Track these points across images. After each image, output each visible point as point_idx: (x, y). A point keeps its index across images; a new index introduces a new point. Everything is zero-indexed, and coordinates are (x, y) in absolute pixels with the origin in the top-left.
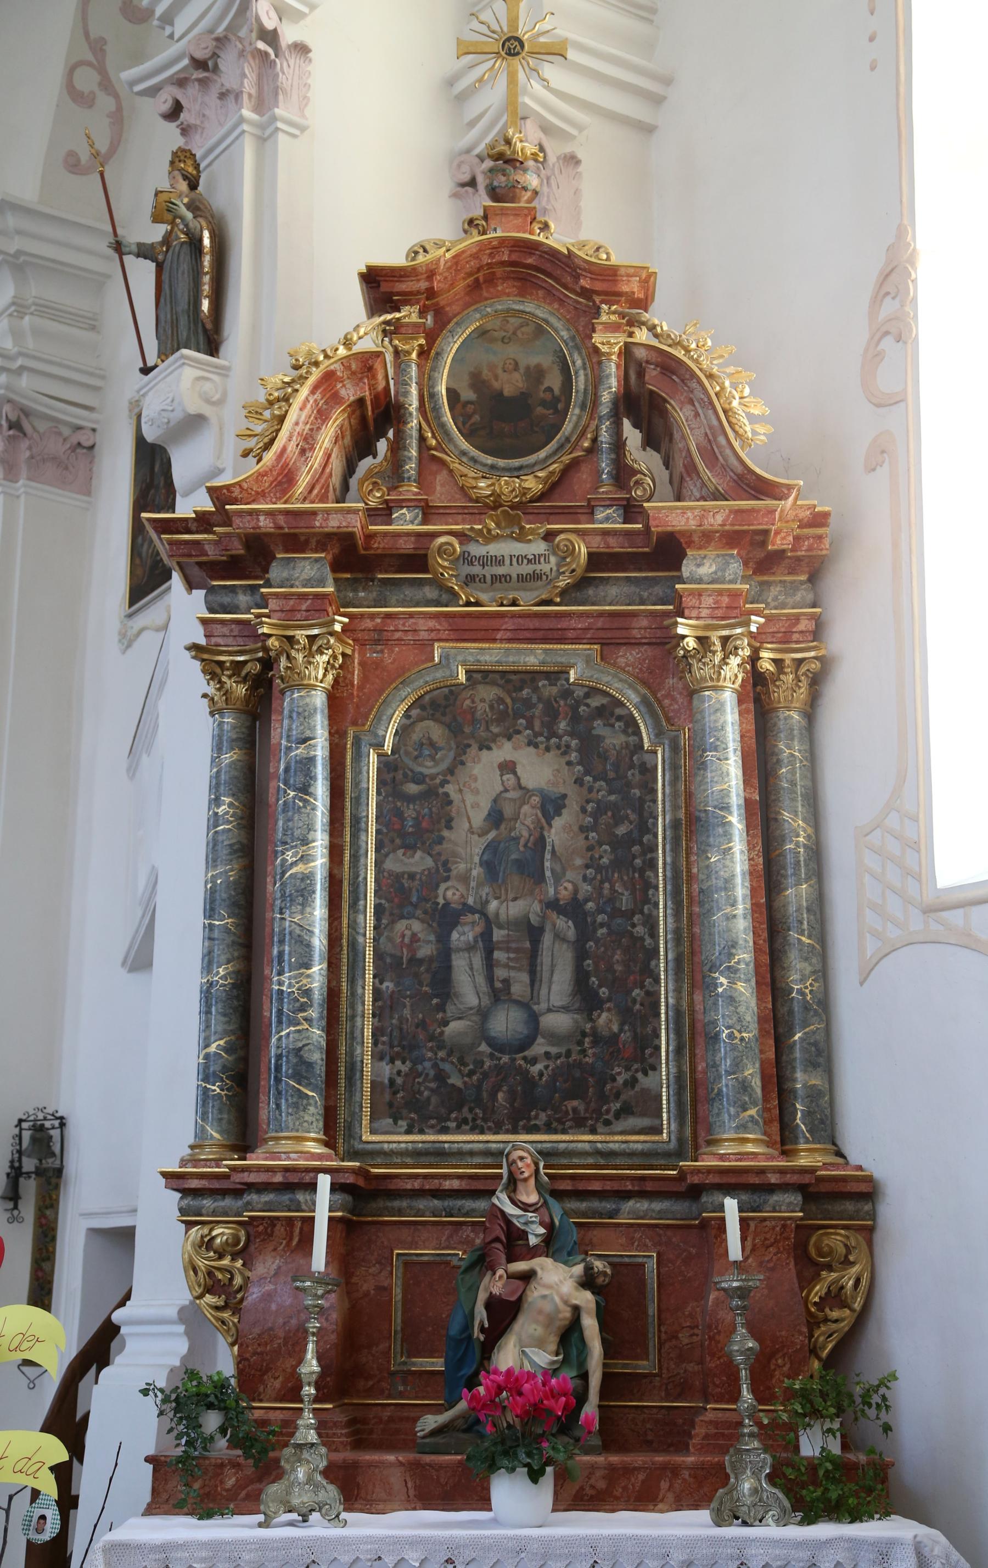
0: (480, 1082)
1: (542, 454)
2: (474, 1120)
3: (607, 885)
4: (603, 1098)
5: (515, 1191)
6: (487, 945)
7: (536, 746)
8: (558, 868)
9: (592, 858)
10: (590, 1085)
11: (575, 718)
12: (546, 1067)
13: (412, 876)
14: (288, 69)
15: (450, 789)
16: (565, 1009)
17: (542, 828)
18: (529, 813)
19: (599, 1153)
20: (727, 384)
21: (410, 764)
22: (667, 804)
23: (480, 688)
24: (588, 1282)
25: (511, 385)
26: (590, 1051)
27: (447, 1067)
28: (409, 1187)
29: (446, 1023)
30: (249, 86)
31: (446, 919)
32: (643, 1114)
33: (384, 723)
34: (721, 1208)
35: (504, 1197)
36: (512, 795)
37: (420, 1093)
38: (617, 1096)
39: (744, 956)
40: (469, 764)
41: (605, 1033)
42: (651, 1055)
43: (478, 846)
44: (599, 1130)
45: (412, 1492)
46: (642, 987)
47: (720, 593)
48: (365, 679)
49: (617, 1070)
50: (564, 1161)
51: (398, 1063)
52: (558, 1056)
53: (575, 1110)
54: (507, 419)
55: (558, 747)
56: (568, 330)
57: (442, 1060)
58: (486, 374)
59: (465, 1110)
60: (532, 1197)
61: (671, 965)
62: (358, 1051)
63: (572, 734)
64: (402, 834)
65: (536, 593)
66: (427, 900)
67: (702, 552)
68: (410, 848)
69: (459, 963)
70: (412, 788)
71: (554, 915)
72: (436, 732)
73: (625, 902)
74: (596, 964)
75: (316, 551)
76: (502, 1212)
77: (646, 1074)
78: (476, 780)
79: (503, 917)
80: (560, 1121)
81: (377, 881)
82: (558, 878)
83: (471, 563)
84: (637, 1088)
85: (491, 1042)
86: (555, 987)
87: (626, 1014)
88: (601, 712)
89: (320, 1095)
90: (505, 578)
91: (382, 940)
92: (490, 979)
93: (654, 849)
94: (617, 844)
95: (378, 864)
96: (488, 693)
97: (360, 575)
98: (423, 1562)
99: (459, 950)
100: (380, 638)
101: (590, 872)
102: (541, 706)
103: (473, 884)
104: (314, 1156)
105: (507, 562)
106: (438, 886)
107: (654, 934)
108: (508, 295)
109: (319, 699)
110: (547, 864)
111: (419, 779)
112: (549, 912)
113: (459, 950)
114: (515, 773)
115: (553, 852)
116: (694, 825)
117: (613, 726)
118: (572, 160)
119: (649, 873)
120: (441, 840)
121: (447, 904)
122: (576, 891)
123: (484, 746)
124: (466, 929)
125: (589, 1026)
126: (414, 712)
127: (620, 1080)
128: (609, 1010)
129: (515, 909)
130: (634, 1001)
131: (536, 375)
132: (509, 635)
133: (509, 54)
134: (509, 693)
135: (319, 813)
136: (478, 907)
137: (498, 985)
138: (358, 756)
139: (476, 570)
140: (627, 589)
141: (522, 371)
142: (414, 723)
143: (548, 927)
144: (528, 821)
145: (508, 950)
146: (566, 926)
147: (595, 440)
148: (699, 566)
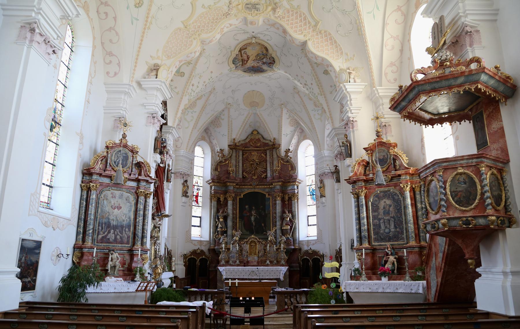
6: (384, 222)
10: (396, 237)
14: (355, 124)
18: (388, 207)
24: (395, 258)
25: (382, 157)
30: (351, 127)
31: (380, 219)
39: (412, 221)
43: (382, 211)
60: (389, 249)
69: (381, 224)
72: (377, 199)
73: (399, 216)
87: (400, 229)
88: (395, 195)
94: (398, 210)
96: (382, 194)
100: (370, 189)
109: (363, 197)
116: (405, 207)
118: (478, 31)
129: (387, 218)
131: (384, 156)
146: (393, 219)
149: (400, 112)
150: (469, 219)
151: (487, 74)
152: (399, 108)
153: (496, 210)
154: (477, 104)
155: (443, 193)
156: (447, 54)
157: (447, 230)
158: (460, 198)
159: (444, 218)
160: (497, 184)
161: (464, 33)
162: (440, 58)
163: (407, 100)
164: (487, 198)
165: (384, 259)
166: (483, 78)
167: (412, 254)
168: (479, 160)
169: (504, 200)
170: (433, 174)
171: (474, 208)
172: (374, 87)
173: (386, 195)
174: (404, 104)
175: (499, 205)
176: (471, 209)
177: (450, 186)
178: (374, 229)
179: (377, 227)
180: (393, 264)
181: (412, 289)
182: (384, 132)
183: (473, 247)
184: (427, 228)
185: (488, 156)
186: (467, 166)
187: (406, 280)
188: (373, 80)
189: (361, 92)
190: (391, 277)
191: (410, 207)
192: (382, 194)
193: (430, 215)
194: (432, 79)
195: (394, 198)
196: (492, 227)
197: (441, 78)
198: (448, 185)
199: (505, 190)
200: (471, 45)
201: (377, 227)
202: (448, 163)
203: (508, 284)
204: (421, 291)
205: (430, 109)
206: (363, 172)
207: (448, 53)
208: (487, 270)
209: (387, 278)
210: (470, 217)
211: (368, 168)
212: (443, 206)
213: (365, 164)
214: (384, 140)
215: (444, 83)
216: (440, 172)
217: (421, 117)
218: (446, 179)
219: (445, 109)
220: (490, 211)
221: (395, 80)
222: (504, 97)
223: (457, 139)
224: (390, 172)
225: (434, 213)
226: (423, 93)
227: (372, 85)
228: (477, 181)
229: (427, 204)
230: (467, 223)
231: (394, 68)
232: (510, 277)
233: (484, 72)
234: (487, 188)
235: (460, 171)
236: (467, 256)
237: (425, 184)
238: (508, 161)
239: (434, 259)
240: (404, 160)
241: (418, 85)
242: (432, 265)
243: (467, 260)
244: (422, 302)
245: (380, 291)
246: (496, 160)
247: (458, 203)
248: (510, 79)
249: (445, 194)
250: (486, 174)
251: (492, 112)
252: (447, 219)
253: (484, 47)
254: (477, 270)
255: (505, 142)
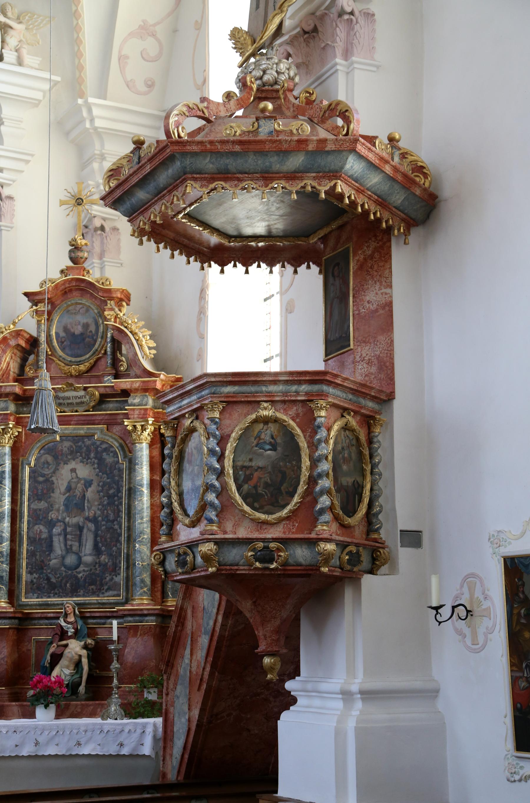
0: (61, 580)
1: (87, 356)
2: (59, 593)
3: (105, 511)
4: (102, 585)
5: (67, 617)
6: (65, 534)
7: (83, 462)
8: (89, 505)
9: (101, 502)
10: (96, 582)
11: (97, 452)
12: (83, 575)
13: (40, 510)
15: (54, 479)
16: (90, 555)
17: (84, 492)
18: (80, 486)
19: (99, 603)
20: (141, 336)
21: (41, 471)
22: (127, 482)
23: (65, 442)
24: (85, 647)
25: (78, 330)
26: (98, 569)
27: (50, 575)
28: (37, 616)
29: (50, 560)
31: (51, 524)
32: (114, 590)
33: (31, 456)
34: (112, 624)
35: (62, 620)
36: (75, 480)
37: (42, 584)
38: (107, 584)
40: (60, 470)
41: (103, 563)
42: (118, 570)
43: (62, 499)
44: (100, 596)
45: (20, 714)
46: (116, 546)
47: (141, 409)
48: (26, 439)
49: (107, 575)
50: (89, 606)
51: (35, 574)
52: (88, 571)
53: (92, 589)
54: (77, 342)
55: (91, 463)
56: (97, 309)
57: (49, 573)
58: (69, 326)
59: (56, 590)
60: (71, 619)
61: (126, 539)
62: (21, 571)
63: (95, 458)
64: (37, 495)
65: (84, 408)
66: (45, 518)
67: (136, 394)
68: (40, 500)
69: (55, 539)
70: (41, 479)
71: (88, 522)
72: (49, 458)
73: (112, 517)
74: (101, 539)
75: (5, 398)
76: (61, 626)
77: (116, 576)
78: (62, 475)
79: (70, 523)
80: (87, 593)
81: (28, 512)
82: (89, 509)
83: (59, 399)
84: (113, 581)
85: (65, 567)
86: (87, 547)
87: (110, 555)
88: (105, 450)
89: (6, 587)
90: (71, 404)
91: (30, 532)
92: (66, 545)
93: (122, 498)
94: (109, 497)
95: (29, 506)
96: (67, 444)
97: (25, 402)
98: (7, 732)
99: (55, 535)
101: (100, 507)
102: (85, 448)
103: (61, 512)
104: (4, 608)
105: (71, 398)
106: (49, 513)
107: (121, 528)
108: (77, 296)
109: (7, 450)
110: (86, 504)
111: (43, 475)
112: (86, 521)
113: (55, 535)
114: (75, 472)
115: (88, 500)
116: (132, 492)
117: (109, 455)
118: (369, 16)
119: (120, 507)
120: (50, 497)
121: (52, 519)
122: (95, 513)
123: (66, 463)
124: (58, 528)
125: (98, 560)
126: (42, 452)
127: (108, 579)
128: (105, 555)
129: (75, 520)
130: (113, 551)
131: (86, 326)
132: (75, 422)
133: (78, 205)
134: (74, 444)
135: (6, 491)
136: (62, 520)
137: (68, 547)
138: (23, 468)
139: (61, 401)
140: (116, 405)
141: (81, 325)
142: (41, 456)
143: (85, 527)
144: (80, 490)
145: (72, 535)
146: (92, 526)
147: (106, 350)
148: (134, 399)
149: (132, 215)
150: (272, 545)
151: (361, 157)
152: (128, 205)
153: (343, 526)
154: (341, 228)
155: (215, 469)
156: (280, 67)
157: (213, 574)
158: (255, 487)
159: (209, 540)
160: (354, 456)
161: (334, 11)
162: (259, 73)
163: (151, 187)
164: (322, 493)
165: (52, 650)
166: (352, 165)
167: (135, 635)
168: (315, 388)
169: (366, 501)
170: (196, 413)
171: (288, 518)
172: (82, 95)
173: (81, 448)
174: (141, 195)
175: (351, 511)
176: (280, 520)
177: (236, 450)
178: (31, 554)
179: (42, 546)
180: (78, 664)
181: (121, 745)
182: (97, 248)
183: (278, 622)
184: (167, 563)
185: (339, 381)
186: (284, 402)
187: (108, 717)
188: (81, 68)
189: (35, 104)
190: (67, 707)
191: (146, 490)
192: (67, 444)
193: (179, 527)
194: (223, 142)
195: (101, 462)
196: (325, 570)
197: (247, 145)
198: (230, 447)
199: (372, 473)
200: (347, 54)
201: (42, 546)
202: (236, 388)
203: (351, 724)
204: (147, 750)
205: (217, 222)
206: (14, 368)
207: (283, 67)
208: (309, 686)
209: (52, 710)
210: (274, 540)
211: (32, 358)
212: (212, 505)
213: (23, 343)
214: (93, 275)
215: (252, 162)
216: (213, 410)
217: (191, 238)
218: (227, 431)
219: (260, 229)
220: (325, 527)
221: (150, 85)
222: (403, 220)
223: (288, 309)
224: (99, 379)
225: (187, 521)
226: (195, 179)
227: (76, 86)
228: (303, 444)
229: (174, 496)
230: (266, 556)
231: (150, 46)
232: (359, 705)
233: (353, 150)
234: (325, 466)
235: (265, 413)
236: (262, 647)
237: (175, 437)
238: (391, 397)
239: (188, 651)
240: (143, 348)
241: (184, 154)
242: (181, 671)
243: (262, 657)
244: (147, 782)
245: (25, 753)
246: (359, 391)
247: (249, 500)
248: (426, 175)
249: (221, 474)
250: (329, 430)
251: (372, 257)
252: (217, 542)
253: (378, 67)
254: (289, 685)
255: (391, 343)
